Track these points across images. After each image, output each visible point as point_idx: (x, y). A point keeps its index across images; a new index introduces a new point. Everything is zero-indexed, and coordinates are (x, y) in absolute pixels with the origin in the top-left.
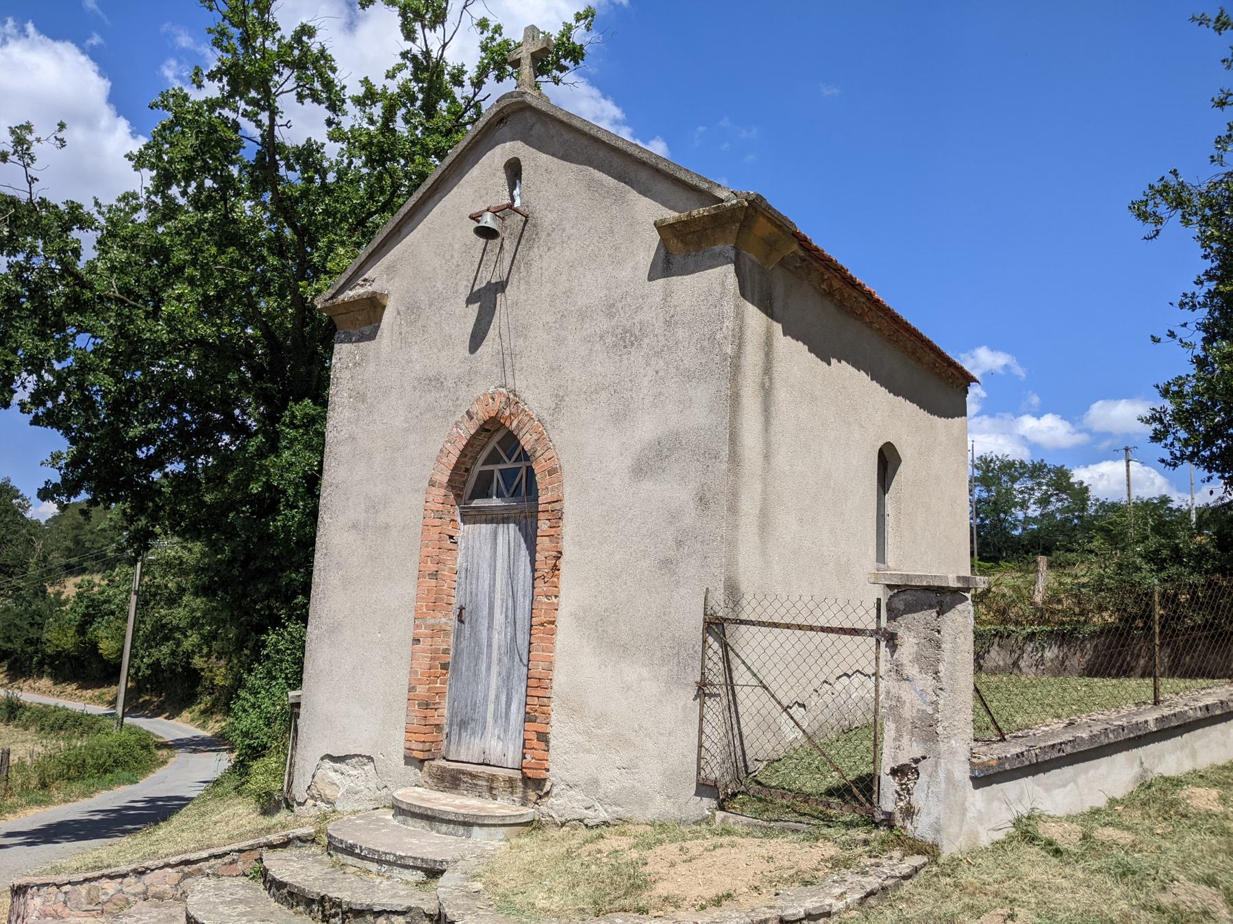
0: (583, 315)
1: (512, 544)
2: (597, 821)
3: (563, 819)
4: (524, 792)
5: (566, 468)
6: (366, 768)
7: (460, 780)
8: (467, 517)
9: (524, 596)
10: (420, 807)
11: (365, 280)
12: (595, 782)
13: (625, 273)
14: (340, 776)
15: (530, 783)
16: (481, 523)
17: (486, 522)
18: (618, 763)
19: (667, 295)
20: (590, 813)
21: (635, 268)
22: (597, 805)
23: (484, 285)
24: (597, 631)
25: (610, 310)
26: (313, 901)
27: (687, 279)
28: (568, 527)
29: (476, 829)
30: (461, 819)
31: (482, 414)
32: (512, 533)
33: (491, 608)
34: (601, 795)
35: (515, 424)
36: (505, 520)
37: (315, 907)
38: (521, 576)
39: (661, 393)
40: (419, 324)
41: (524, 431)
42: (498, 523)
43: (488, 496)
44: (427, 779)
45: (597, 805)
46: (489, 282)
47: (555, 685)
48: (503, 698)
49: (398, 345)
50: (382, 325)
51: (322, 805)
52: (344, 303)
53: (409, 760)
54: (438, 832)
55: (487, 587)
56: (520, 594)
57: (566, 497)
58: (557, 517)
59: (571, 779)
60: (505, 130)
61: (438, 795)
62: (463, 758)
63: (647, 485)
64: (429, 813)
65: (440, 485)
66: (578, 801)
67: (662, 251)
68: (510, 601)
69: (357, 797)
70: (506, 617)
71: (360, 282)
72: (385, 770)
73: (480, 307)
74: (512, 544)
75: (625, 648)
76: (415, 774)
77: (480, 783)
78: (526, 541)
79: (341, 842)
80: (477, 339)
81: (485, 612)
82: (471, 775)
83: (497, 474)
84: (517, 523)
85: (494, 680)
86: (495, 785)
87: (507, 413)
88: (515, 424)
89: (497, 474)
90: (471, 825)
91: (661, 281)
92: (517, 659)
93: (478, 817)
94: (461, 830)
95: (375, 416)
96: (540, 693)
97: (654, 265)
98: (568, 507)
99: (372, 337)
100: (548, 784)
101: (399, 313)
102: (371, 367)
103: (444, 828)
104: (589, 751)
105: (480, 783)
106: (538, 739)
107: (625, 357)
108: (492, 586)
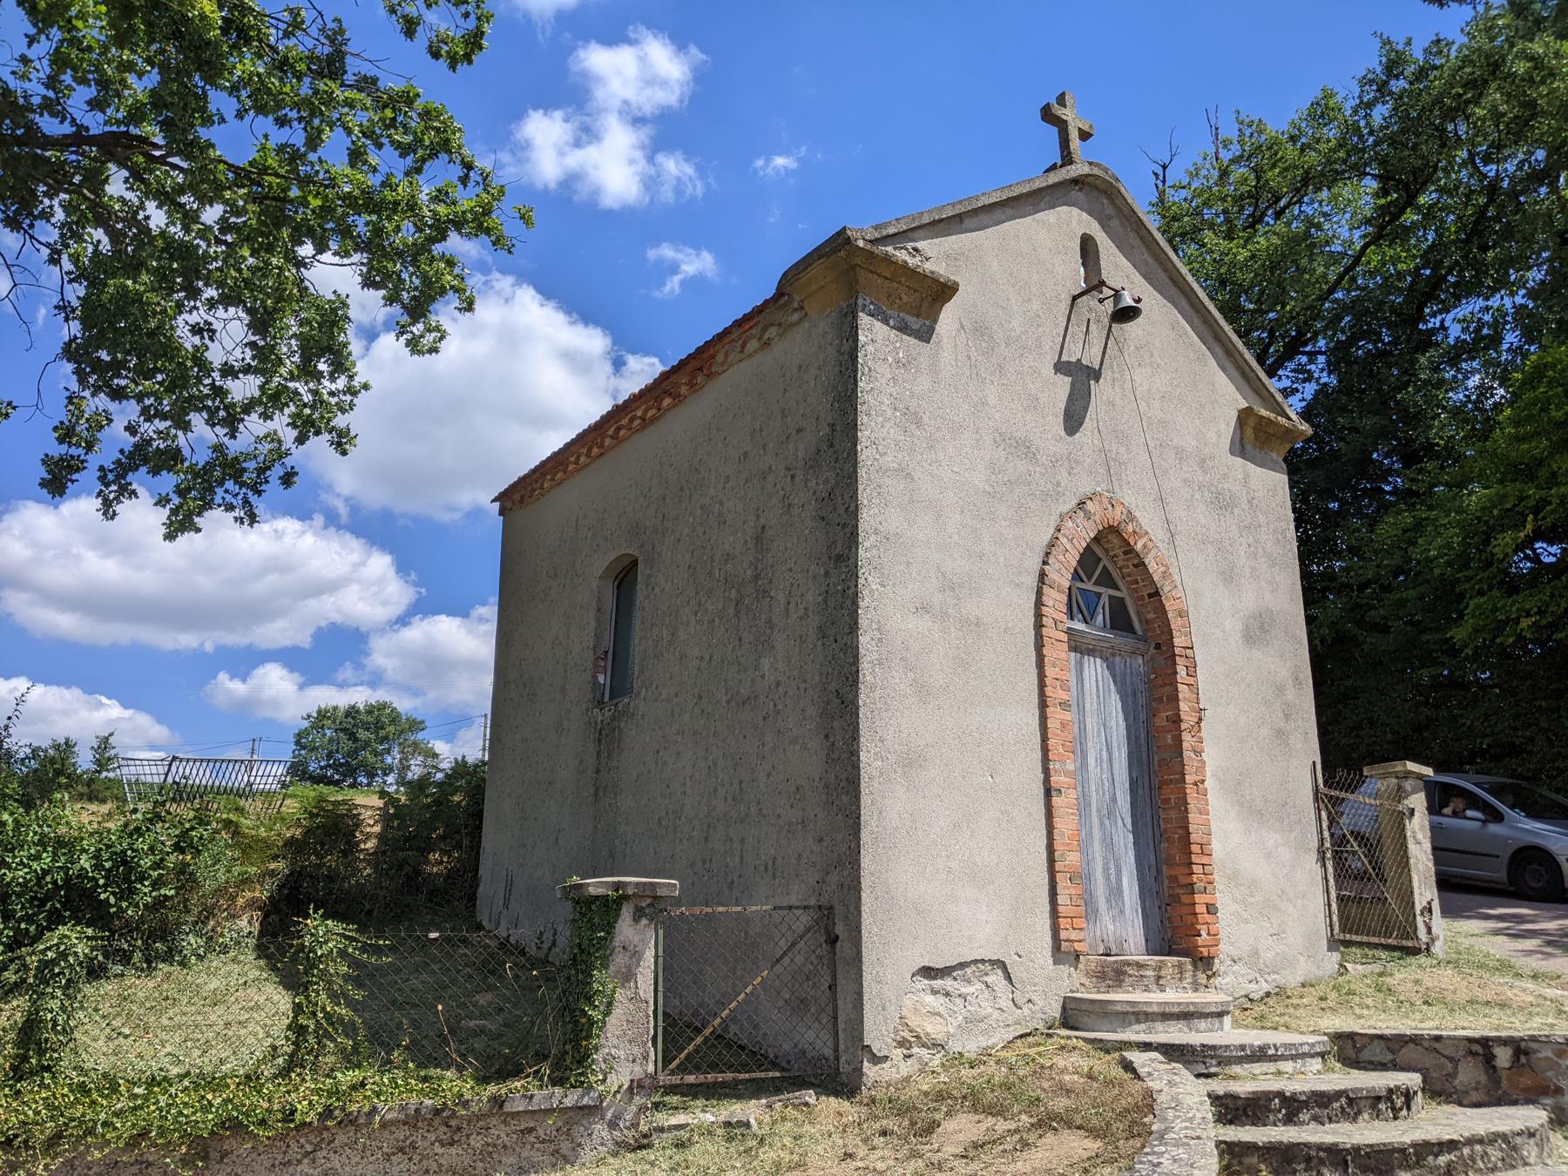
6: (989, 979)
7: (1125, 973)
10: (1179, 1004)
11: (916, 249)
14: (942, 999)
26: (1378, 1098)
36: (1091, 652)
37: (1382, 1106)
44: (1084, 980)
48: (1112, 871)
51: (924, 1052)
52: (887, 259)
54: (1197, 1031)
56: (1115, 745)
58: (1192, 670)
60: (1075, 194)
64: (1192, 1009)
69: (983, 1026)
71: (910, 245)
79: (1243, 1047)
80: (1073, 420)
83: (1105, 600)
84: (1106, 659)
86: (1163, 973)
89: (1105, 600)
92: (1120, 823)
101: (962, 327)
102: (924, 383)
104: (1246, 921)
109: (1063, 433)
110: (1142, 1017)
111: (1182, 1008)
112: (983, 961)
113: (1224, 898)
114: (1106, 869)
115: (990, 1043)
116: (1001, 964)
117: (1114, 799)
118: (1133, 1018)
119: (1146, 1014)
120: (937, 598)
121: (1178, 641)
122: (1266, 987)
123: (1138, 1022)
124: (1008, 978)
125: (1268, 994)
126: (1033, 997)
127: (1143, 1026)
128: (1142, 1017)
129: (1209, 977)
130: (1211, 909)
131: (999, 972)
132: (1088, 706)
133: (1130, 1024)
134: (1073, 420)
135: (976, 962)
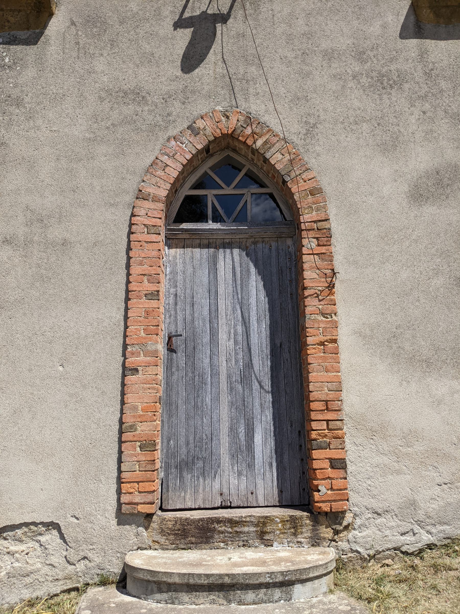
0: (329, 55)
1: (238, 269)
2: (419, 545)
3: (372, 552)
4: (314, 530)
5: (328, 189)
7: (214, 530)
8: (172, 241)
9: (258, 321)
10: (208, 576)
12: (413, 504)
13: (375, 29)
15: (322, 519)
16: (193, 247)
17: (200, 246)
18: (439, 480)
19: (423, 54)
20: (408, 538)
21: (384, 26)
22: (417, 528)
23: (198, 13)
24: (391, 348)
25: (360, 56)
27: (442, 43)
28: (339, 249)
29: (298, 588)
30: (280, 579)
31: (209, 129)
32: (237, 258)
33: (214, 334)
34: (421, 515)
35: (259, 143)
38: (253, 301)
39: (431, 131)
40: (106, 38)
41: (273, 150)
42: (217, 247)
43: (202, 218)
44: (158, 538)
45: (417, 528)
46: (204, 13)
47: (346, 408)
48: (242, 430)
49: (75, 54)
50: (47, 32)
53: (123, 517)
54: (240, 603)
55: (206, 312)
57: (332, 217)
58: (325, 237)
59: (378, 506)
61: (177, 554)
62: (189, 504)
63: (429, 210)
64: (227, 580)
65: (155, 199)
66: (391, 528)
67: (412, 18)
68: (240, 329)
69: (28, 580)
70: (236, 343)
72: (81, 536)
73: (193, 32)
74: (238, 269)
75: (428, 362)
76: (137, 535)
77: (246, 529)
78: (256, 266)
81: (206, 339)
82: (232, 522)
85: (224, 412)
86: (268, 528)
87: (248, 131)
88: (259, 143)
90: (291, 583)
91: (414, 42)
92: (256, 386)
93: (301, 571)
94: (277, 593)
95: (39, 122)
96: (330, 416)
97: (404, 27)
98: (336, 226)
99: (33, 40)
100: (348, 518)
101: (73, 23)
103: (250, 596)
104: (398, 472)
105: (246, 529)
106: (332, 467)
107: (385, 96)
108: (214, 312)
109: (179, 73)
110: (173, 588)
111: (211, 580)
112: (35, 524)
113: (357, 451)
114: (233, 430)
115: (34, 595)
116: (57, 526)
117: (249, 365)
118: (155, 587)
119: (169, 584)
120: (21, 231)
121: (307, 217)
122: (426, 538)
123: (160, 591)
124: (62, 537)
125: (430, 546)
126: (90, 555)
127: (165, 596)
128: (164, 588)
129: (337, 532)
130: (339, 464)
131: (55, 532)
132: (221, 290)
133: (152, 592)
134: (192, 60)
135: (26, 524)
